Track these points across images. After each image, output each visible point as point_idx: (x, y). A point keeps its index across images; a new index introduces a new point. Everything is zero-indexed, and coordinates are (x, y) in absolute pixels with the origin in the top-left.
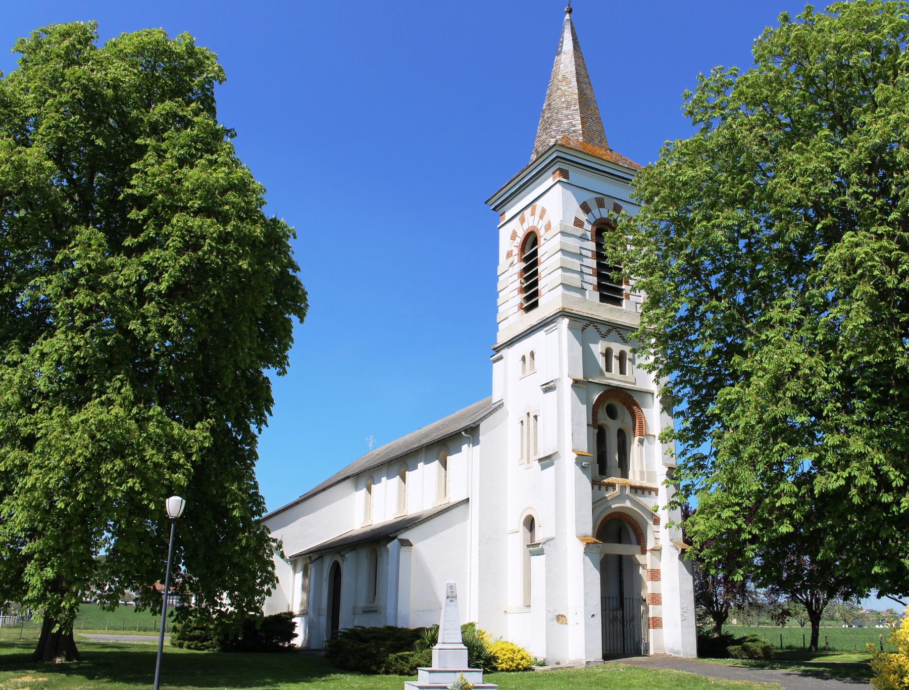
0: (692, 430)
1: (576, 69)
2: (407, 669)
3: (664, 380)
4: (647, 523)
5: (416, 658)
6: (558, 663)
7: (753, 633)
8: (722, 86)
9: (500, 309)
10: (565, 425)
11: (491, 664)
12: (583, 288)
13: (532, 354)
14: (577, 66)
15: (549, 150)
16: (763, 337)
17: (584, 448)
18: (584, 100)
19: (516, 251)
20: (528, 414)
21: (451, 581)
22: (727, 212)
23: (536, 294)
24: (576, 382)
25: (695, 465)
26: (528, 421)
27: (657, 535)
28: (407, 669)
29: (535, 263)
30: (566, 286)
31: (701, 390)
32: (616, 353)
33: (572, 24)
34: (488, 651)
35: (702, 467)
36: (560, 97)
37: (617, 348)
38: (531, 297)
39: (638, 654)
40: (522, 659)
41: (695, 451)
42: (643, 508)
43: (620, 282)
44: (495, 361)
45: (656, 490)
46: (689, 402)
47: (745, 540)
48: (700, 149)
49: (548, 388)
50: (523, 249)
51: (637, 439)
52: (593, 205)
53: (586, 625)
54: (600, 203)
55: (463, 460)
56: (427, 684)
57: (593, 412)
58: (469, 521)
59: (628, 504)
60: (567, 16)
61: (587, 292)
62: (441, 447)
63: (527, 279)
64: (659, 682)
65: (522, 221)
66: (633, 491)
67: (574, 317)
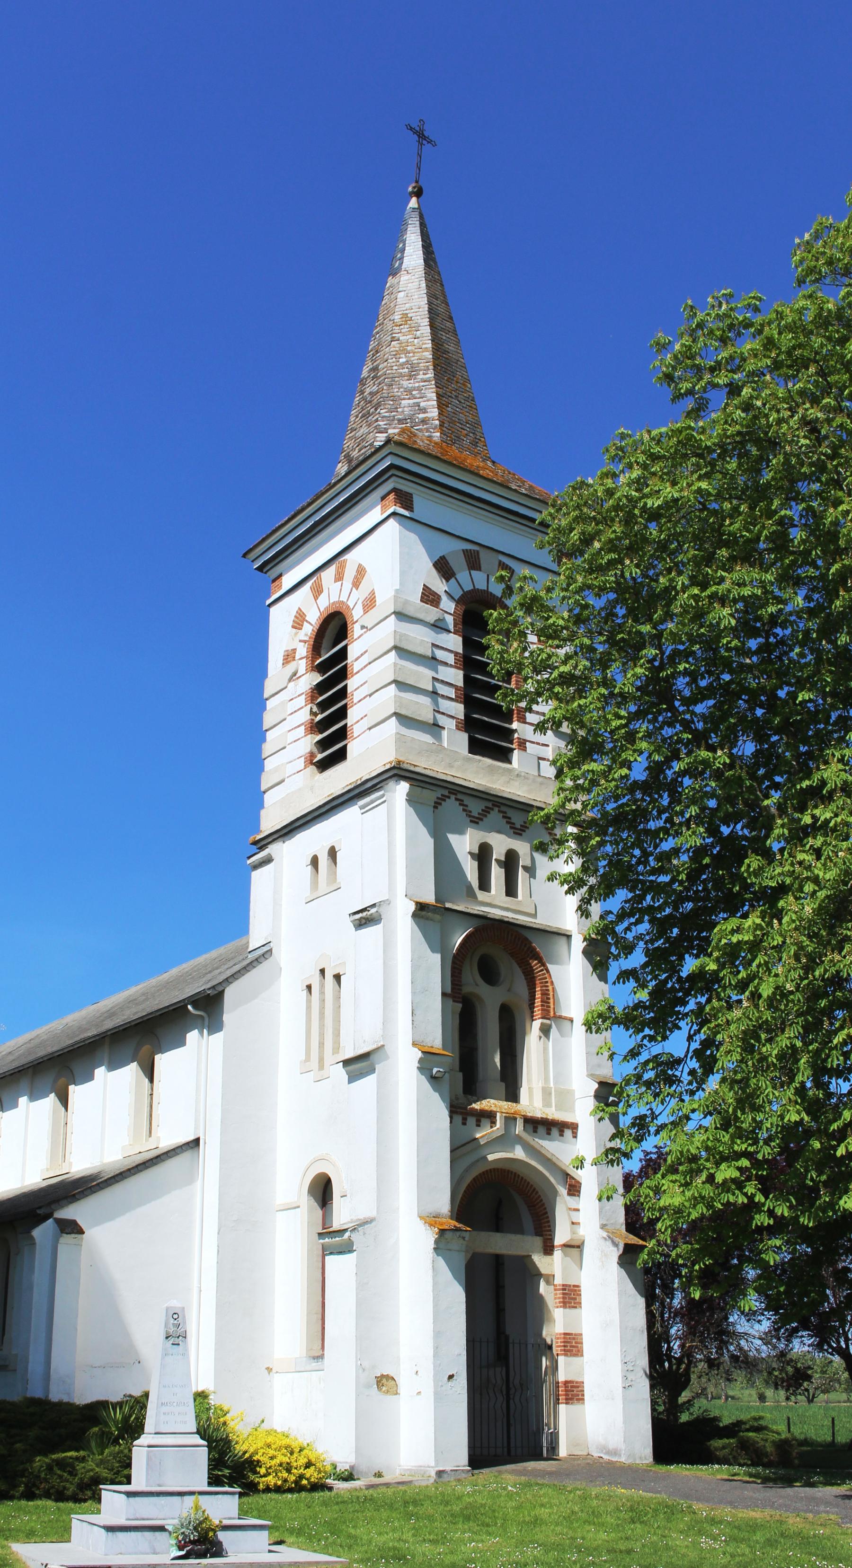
0: (649, 1008)
1: (430, 303)
2: (71, 1489)
3: (596, 909)
4: (555, 1193)
5: (91, 1464)
6: (379, 1475)
7: (753, 1414)
8: (731, 327)
9: (269, 764)
10: (397, 993)
11: (245, 1477)
12: (436, 725)
13: (333, 853)
14: (432, 296)
15: (373, 454)
16: (807, 820)
17: (435, 1039)
18: (444, 363)
19: (303, 651)
20: (322, 971)
21: (175, 1304)
22: (741, 571)
23: (343, 734)
24: (422, 911)
25: (657, 1076)
26: (322, 986)
27: (575, 1216)
28: (71, 1489)
29: (343, 674)
30: (404, 720)
31: (674, 928)
32: (498, 853)
33: (421, 217)
34: (239, 1448)
35: (671, 1081)
36: (396, 355)
37: (500, 844)
38: (331, 741)
39: (537, 1456)
40: (308, 1465)
41: (656, 1049)
42: (548, 1161)
43: (508, 717)
44: (256, 867)
45: (574, 1127)
46: (647, 952)
47: (760, 1229)
48: (687, 449)
49: (365, 919)
50: (316, 647)
51: (537, 1024)
52: (458, 564)
53: (438, 1397)
54: (473, 561)
55: (189, 1063)
56: (122, 1521)
57: (453, 969)
58: (199, 1183)
59: (519, 1153)
60: (413, 203)
61: (445, 733)
62: (143, 1036)
63: (323, 706)
64: (595, 1513)
65: (317, 591)
66: (530, 1127)
67: (419, 781)
